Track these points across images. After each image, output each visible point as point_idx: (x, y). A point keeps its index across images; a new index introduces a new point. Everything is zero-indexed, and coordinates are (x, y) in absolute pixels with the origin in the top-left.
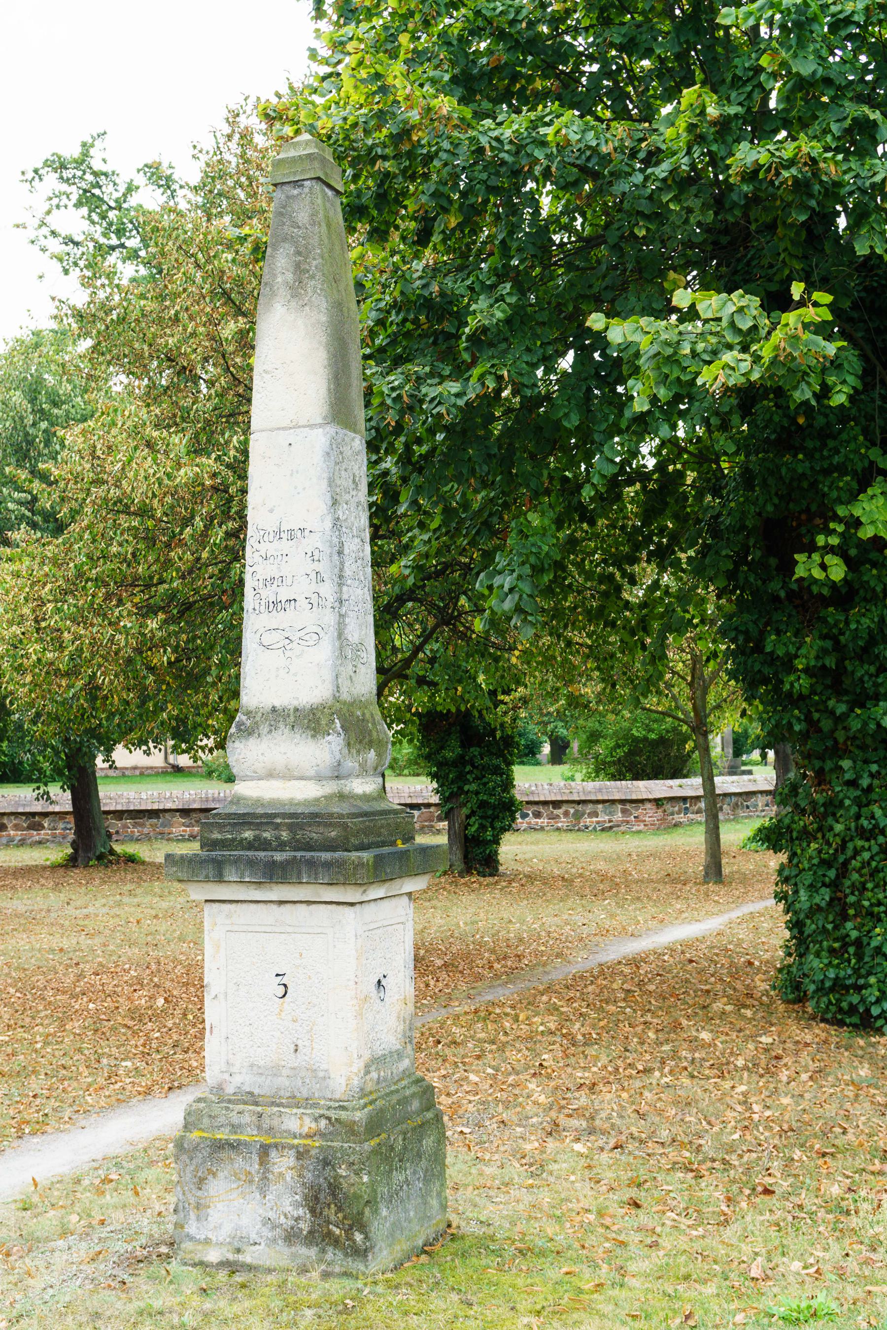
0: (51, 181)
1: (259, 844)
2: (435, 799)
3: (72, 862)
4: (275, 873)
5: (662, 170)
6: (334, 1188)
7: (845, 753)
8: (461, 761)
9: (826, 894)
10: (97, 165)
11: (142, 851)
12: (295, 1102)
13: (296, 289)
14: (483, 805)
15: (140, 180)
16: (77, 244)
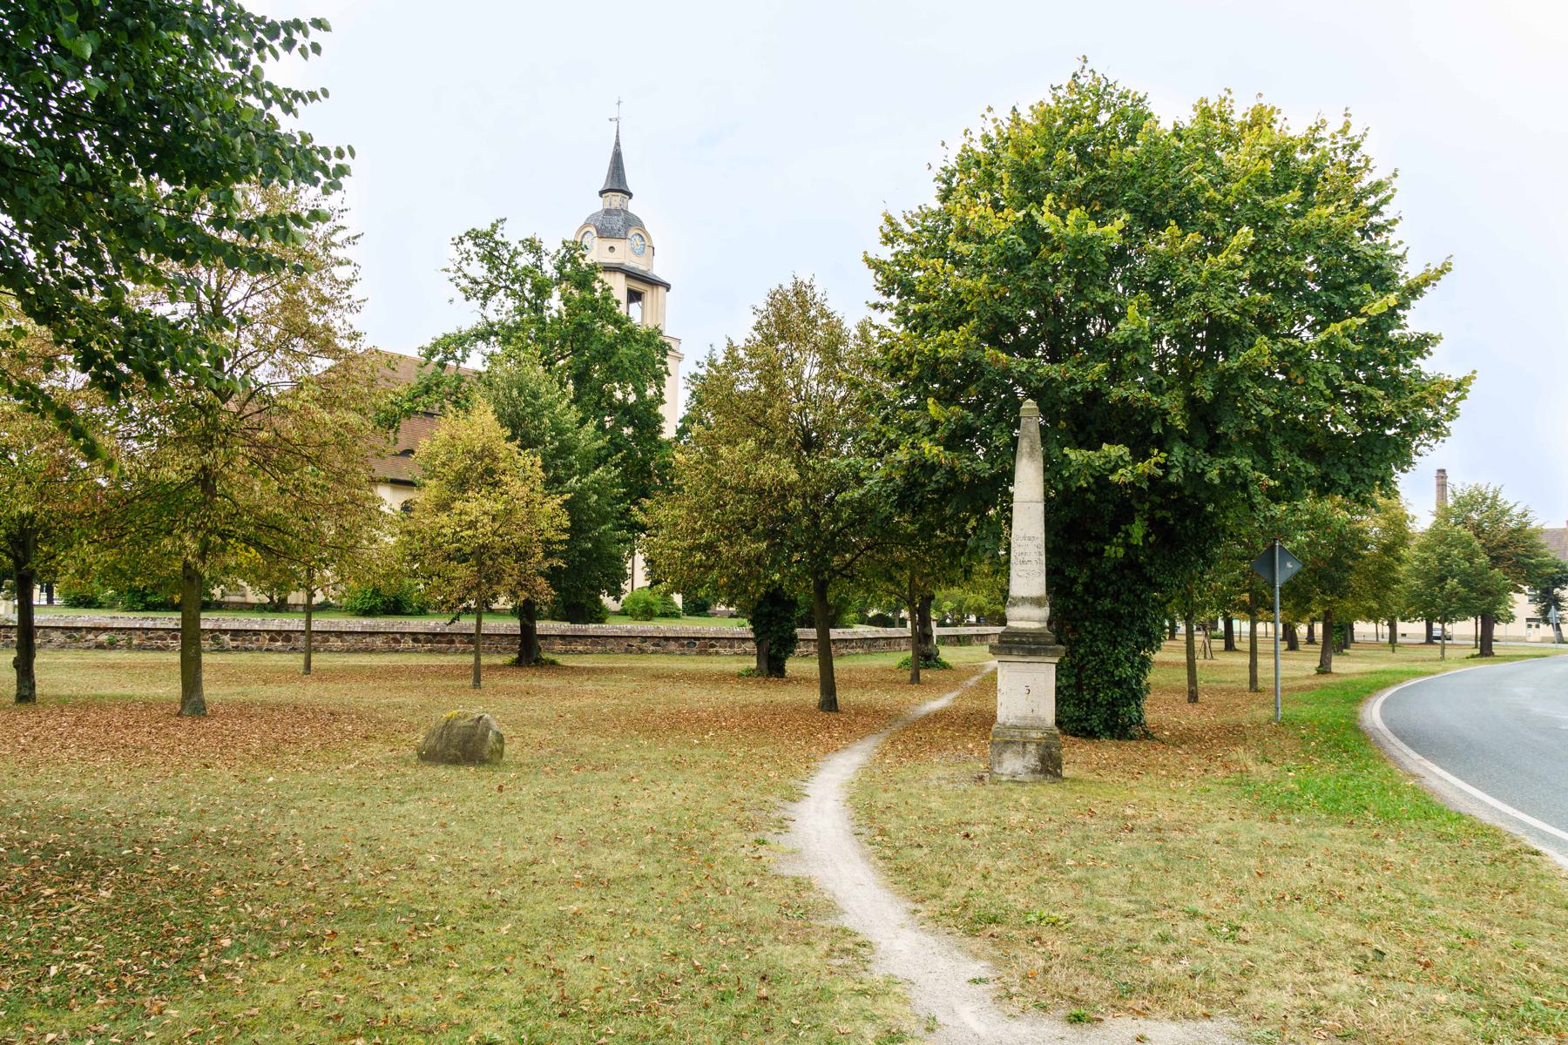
0: (468, 244)
1: (1021, 642)
2: (751, 635)
3: (518, 663)
4: (1031, 652)
5: (1078, 388)
6: (1050, 755)
7: (1087, 619)
8: (770, 614)
9: (1073, 681)
10: (497, 237)
11: (560, 659)
12: (1033, 728)
13: (1031, 455)
14: (780, 638)
15: (520, 249)
16: (477, 283)
